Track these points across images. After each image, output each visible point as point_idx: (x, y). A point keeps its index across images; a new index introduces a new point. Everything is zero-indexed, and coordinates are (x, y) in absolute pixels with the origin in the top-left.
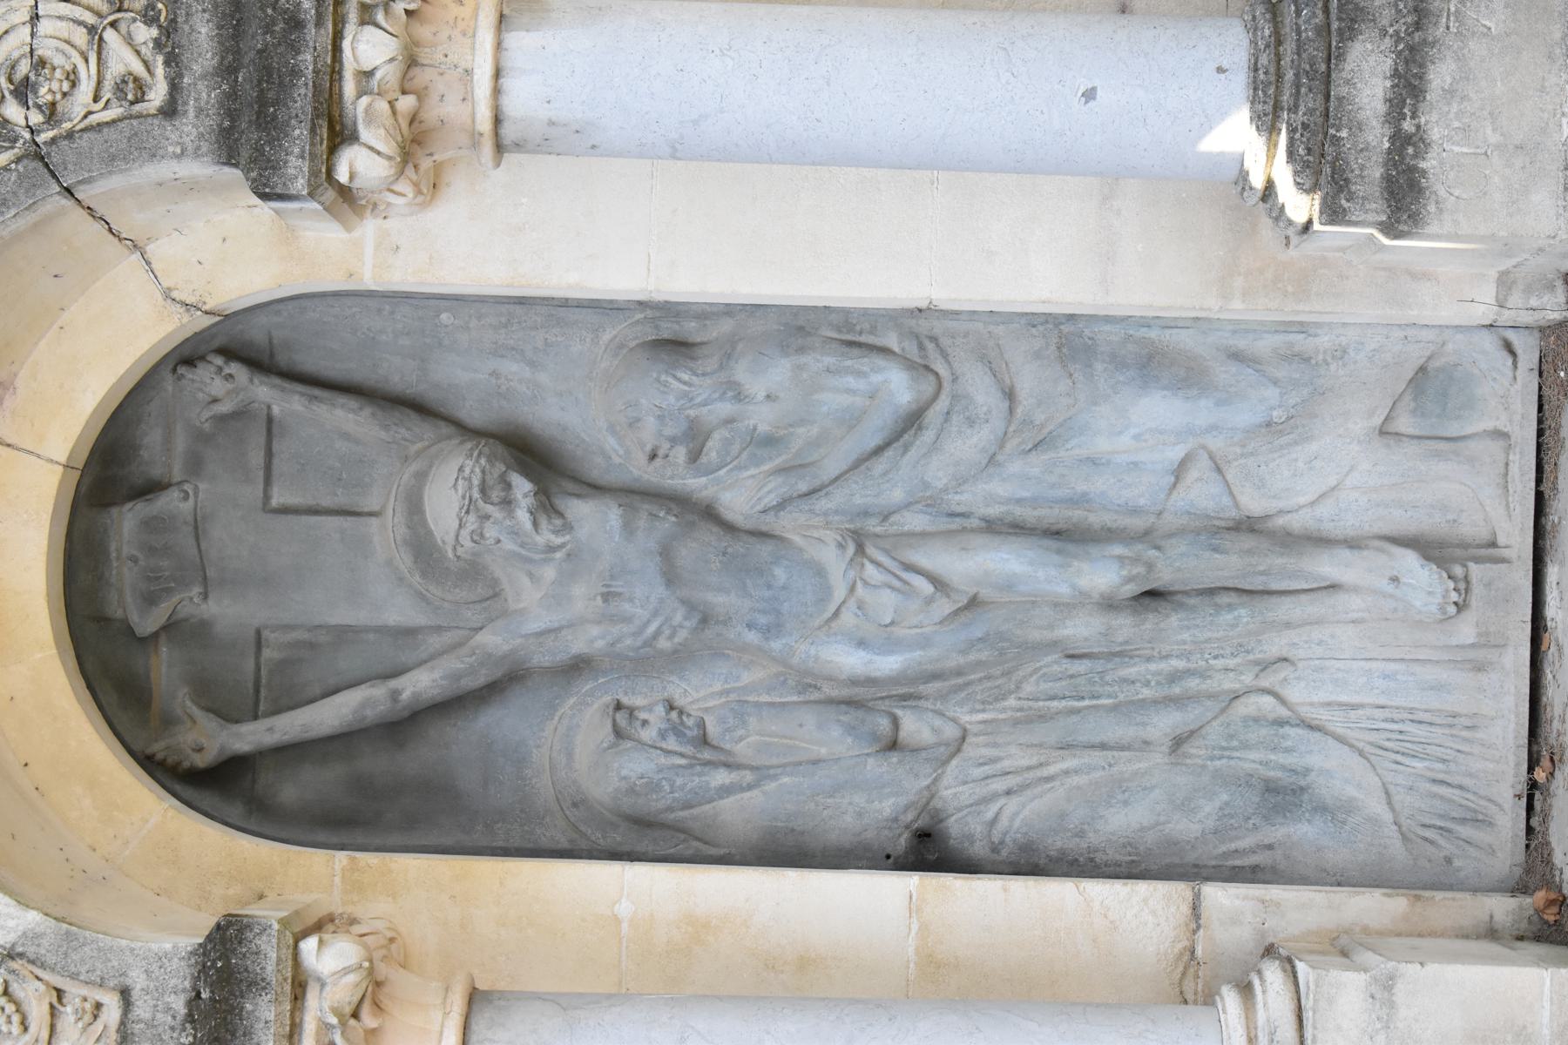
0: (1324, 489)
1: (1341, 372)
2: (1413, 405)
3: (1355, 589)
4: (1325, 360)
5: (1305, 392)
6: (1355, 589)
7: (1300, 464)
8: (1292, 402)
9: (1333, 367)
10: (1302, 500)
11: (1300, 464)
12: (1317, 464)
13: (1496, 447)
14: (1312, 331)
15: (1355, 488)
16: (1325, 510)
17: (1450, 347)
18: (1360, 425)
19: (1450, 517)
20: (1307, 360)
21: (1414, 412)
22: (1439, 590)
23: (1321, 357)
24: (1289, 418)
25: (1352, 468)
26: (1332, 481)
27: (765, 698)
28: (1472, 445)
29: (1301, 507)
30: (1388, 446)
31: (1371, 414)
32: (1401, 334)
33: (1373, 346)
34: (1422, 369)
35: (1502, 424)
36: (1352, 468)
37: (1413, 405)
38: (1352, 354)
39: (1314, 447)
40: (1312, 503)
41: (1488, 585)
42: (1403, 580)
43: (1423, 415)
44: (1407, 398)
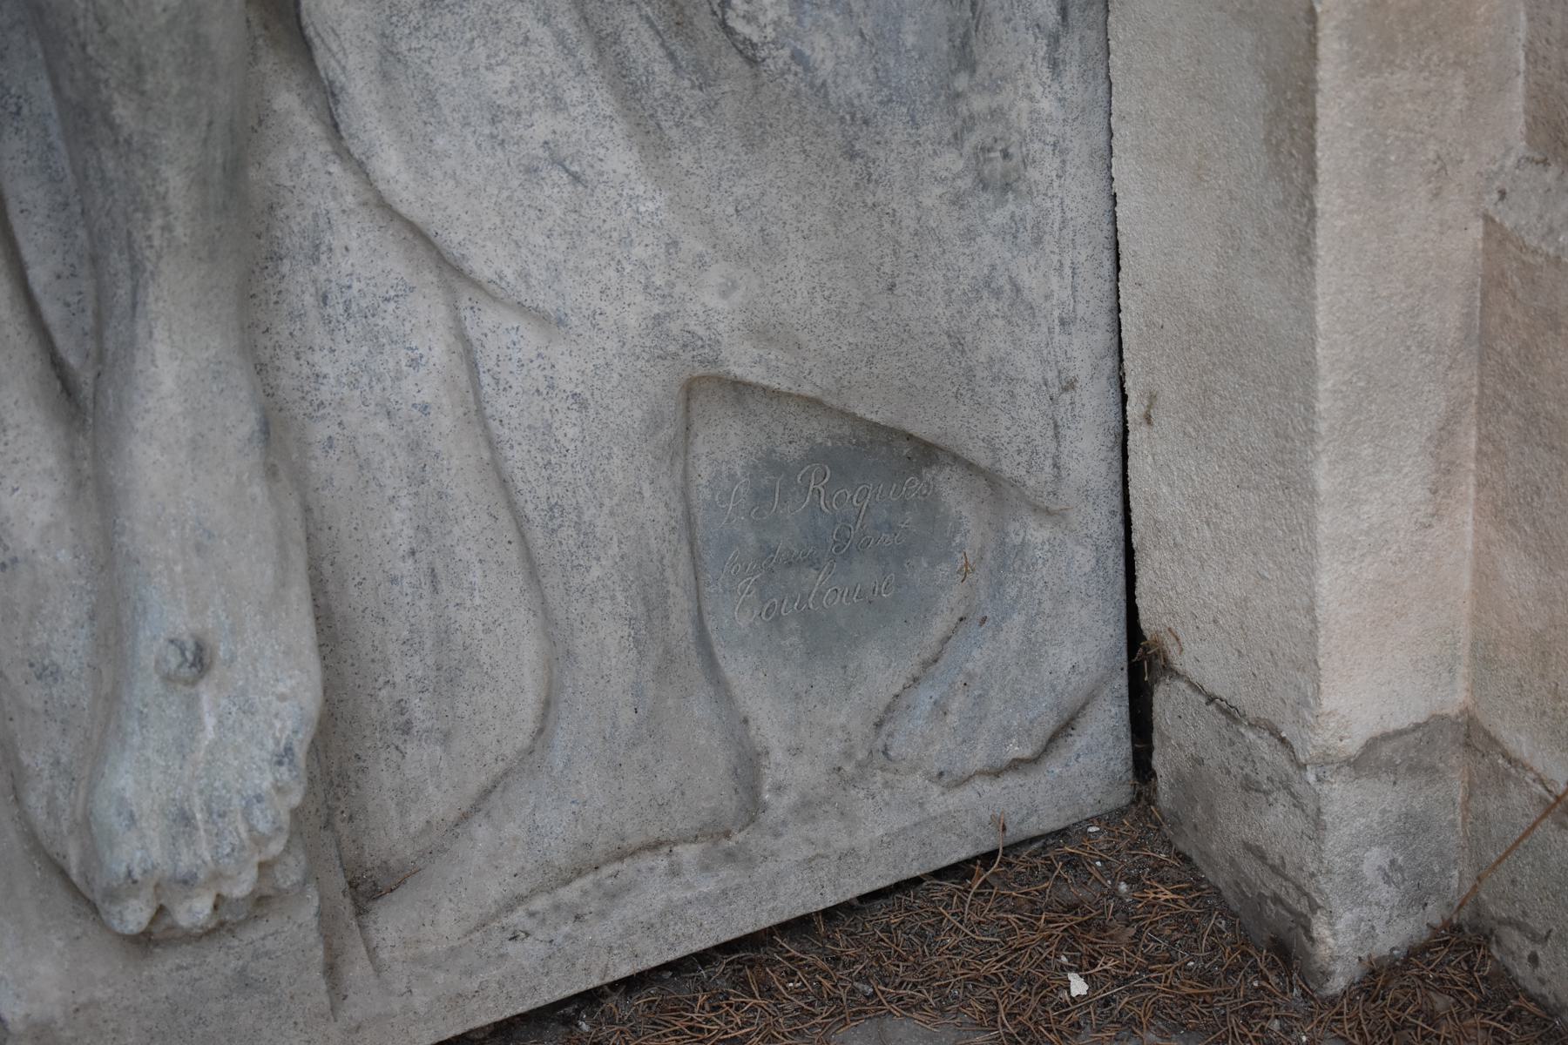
0: (453, 239)
1: (931, 196)
2: (793, 452)
3: (95, 487)
4: (970, 123)
5: (857, 86)
6: (95, 487)
7: (543, 126)
8: (819, 49)
9: (951, 161)
10: (390, 165)
11: (543, 126)
12: (554, 190)
13: (712, 789)
14: (1072, 45)
15: (468, 352)
16: (360, 257)
17: (1038, 534)
18: (715, 306)
19: (419, 709)
20: (964, 57)
21: (771, 463)
22: (198, 854)
23: (979, 103)
24: (750, 55)
25: (551, 322)
26: (487, 260)
27: (82, 793)
28: (701, 707)
29: (360, 168)
30: (655, 422)
31: (762, 333)
32: (1081, 369)
33: (1027, 279)
34: (927, 453)
35: (791, 773)
36: (540, 318)
37: (793, 452)
38: (999, 217)
39: (620, 160)
40: (384, 207)
41: (244, 982)
42: (206, 694)
43: (761, 496)
44: (816, 430)
